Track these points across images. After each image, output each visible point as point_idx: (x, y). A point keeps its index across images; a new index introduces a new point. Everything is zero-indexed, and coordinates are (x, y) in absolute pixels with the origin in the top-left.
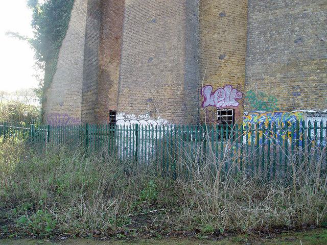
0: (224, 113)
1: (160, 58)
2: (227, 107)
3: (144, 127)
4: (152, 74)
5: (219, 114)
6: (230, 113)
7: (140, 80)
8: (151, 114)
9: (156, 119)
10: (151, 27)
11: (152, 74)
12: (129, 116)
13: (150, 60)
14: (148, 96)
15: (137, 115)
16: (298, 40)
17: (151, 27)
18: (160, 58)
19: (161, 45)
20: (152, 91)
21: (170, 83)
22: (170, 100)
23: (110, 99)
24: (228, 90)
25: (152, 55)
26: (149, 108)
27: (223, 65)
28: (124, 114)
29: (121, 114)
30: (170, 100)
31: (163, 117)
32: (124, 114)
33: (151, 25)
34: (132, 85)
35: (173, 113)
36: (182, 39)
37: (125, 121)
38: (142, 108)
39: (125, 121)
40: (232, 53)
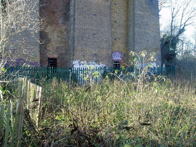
0: (116, 62)
1: (100, 35)
2: (117, 60)
3: (77, 69)
4: (96, 42)
5: (115, 62)
6: (119, 62)
7: (89, 43)
8: (96, 62)
9: (99, 64)
10: (93, 17)
11: (96, 42)
12: (82, 62)
13: (94, 34)
14: (94, 52)
15: (88, 62)
16: (147, 41)
17: (93, 17)
18: (100, 35)
19: (100, 29)
20: (96, 50)
21: (105, 48)
22: (106, 56)
23: (48, 50)
24: (118, 53)
25: (95, 32)
26: (95, 58)
27: (116, 42)
28: (79, 61)
29: (77, 61)
30: (106, 56)
31: (103, 63)
32: (79, 61)
33: (93, 17)
34: (84, 46)
35: (108, 62)
36: (72, 19)
37: (80, 65)
38: (91, 58)
39: (80, 65)
40: (119, 39)
